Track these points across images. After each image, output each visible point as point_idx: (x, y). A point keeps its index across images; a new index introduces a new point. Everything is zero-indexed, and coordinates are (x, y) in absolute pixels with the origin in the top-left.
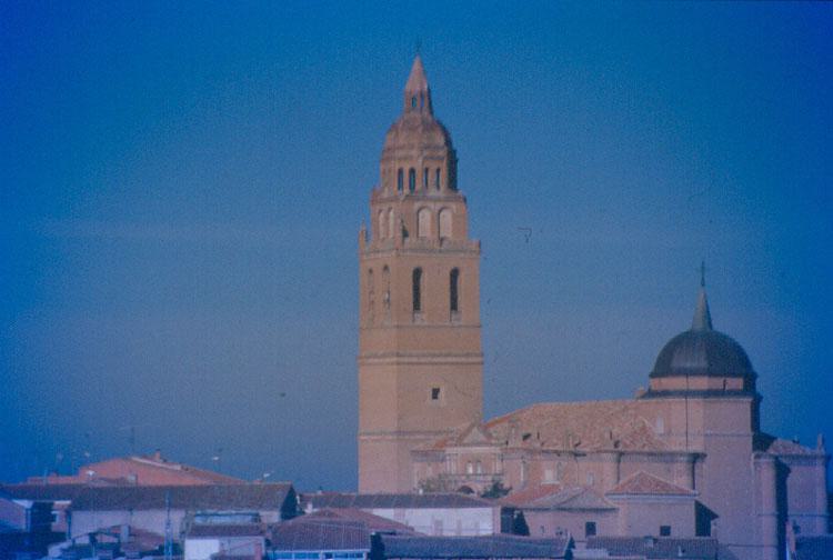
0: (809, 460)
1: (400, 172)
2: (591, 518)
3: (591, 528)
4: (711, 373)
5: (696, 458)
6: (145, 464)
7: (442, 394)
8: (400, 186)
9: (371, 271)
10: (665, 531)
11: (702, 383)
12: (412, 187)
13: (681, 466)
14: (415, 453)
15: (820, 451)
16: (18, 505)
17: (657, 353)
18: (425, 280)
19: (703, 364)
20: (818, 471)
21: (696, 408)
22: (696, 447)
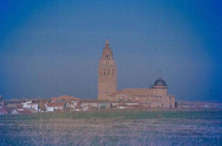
0: (173, 97)
1: (106, 55)
2: (149, 105)
3: (149, 106)
4: (163, 85)
5: (161, 97)
6: (201, 105)
7: (112, 87)
8: (106, 57)
9: (101, 69)
10: (159, 106)
11: (162, 87)
12: (108, 57)
13: (160, 98)
14: (109, 95)
15: (174, 96)
16: (79, 109)
17: (154, 82)
18: (114, 71)
19: (162, 84)
20: (174, 98)
21: (161, 90)
22: (161, 95)
